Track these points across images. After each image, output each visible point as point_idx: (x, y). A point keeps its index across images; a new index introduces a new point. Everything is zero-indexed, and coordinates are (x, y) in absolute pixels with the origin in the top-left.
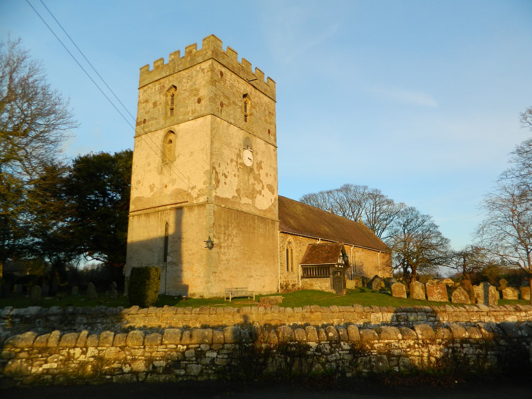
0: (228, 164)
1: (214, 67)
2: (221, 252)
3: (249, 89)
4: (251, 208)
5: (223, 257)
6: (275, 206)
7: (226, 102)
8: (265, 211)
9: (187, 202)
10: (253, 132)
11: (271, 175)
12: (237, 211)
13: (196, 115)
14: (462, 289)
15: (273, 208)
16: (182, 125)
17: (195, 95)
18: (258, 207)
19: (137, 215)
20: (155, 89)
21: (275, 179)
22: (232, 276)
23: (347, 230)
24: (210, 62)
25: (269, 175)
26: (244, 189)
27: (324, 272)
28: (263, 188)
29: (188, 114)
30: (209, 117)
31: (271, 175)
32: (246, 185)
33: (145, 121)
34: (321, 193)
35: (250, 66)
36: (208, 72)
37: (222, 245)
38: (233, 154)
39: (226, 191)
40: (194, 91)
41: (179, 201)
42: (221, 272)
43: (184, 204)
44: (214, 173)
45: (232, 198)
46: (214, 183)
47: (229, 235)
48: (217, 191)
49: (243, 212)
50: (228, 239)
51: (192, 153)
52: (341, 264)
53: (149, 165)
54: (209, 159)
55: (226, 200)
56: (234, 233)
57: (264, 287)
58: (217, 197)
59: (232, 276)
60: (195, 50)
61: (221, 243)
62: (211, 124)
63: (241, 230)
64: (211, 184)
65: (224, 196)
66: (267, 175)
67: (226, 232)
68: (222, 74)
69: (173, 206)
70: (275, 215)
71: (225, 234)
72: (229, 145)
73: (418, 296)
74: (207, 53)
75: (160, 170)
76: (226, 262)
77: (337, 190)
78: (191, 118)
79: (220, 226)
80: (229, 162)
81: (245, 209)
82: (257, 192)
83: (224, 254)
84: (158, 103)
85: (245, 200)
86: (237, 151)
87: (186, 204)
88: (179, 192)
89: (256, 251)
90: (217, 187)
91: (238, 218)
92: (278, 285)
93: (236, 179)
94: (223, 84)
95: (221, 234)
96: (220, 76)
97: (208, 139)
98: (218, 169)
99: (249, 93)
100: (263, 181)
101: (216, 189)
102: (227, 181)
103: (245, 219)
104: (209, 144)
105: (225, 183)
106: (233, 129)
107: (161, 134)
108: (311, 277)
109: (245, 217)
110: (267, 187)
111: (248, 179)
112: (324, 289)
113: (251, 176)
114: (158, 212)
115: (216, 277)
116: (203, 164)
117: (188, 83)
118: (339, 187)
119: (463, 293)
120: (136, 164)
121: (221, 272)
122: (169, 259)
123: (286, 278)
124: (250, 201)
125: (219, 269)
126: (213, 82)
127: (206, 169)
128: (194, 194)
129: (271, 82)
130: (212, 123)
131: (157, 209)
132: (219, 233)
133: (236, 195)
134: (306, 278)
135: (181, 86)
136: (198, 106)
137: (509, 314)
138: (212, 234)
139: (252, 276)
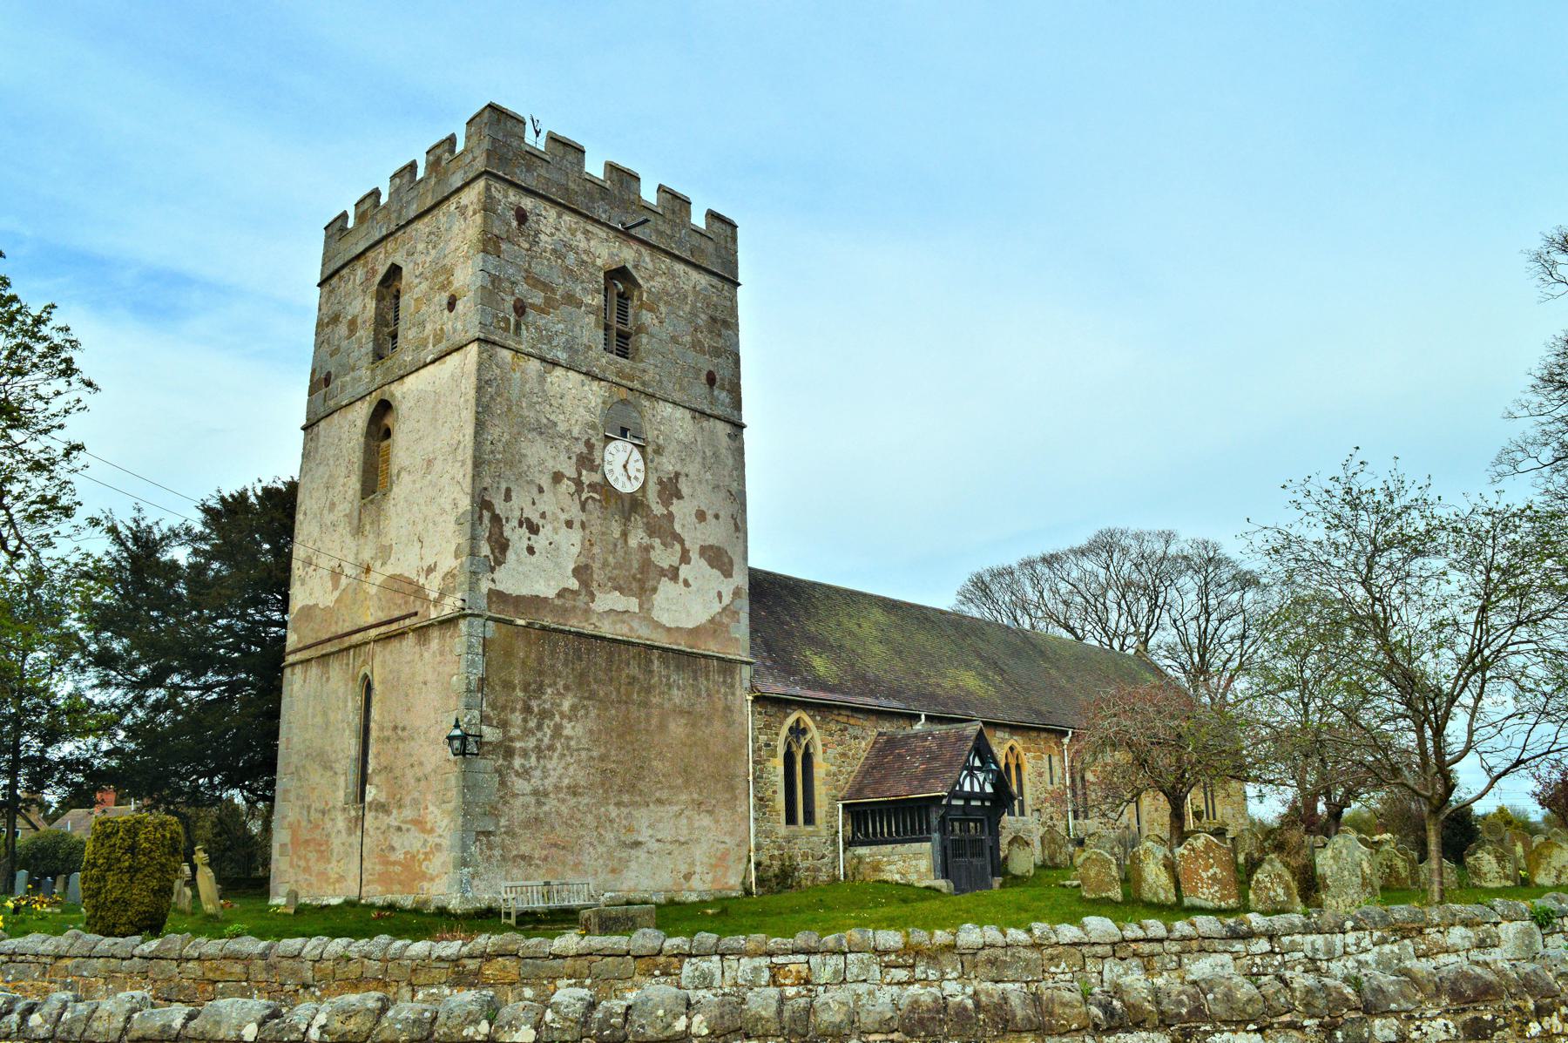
0: (541, 490)
2: (510, 767)
3: (627, 254)
4: (635, 624)
5: (519, 785)
6: (736, 613)
7: (537, 298)
8: (695, 632)
10: (643, 384)
11: (717, 517)
12: (579, 635)
13: (443, 346)
14: (1278, 865)
15: (725, 620)
17: (443, 287)
18: (666, 619)
19: (302, 662)
22: (555, 845)
23: (1063, 682)
24: (481, 183)
25: (709, 517)
26: (605, 564)
27: (913, 825)
29: (426, 346)
31: (717, 517)
32: (614, 552)
33: (327, 381)
34: (1030, 564)
37: (518, 745)
38: (563, 456)
39: (538, 573)
41: (397, 614)
42: (510, 832)
43: (407, 622)
44: (486, 521)
45: (559, 595)
46: (485, 550)
47: (545, 715)
48: (496, 575)
49: (603, 638)
50: (539, 727)
51: (430, 462)
52: (982, 796)
54: (469, 479)
55: (536, 603)
56: (566, 705)
57: (688, 877)
58: (497, 596)
59: (555, 845)
61: (512, 740)
63: (592, 696)
65: (525, 591)
66: (701, 516)
67: (534, 704)
68: (522, 216)
69: (383, 629)
70: (738, 641)
71: (527, 709)
72: (545, 430)
73: (1156, 894)
75: (356, 522)
76: (533, 800)
77: (1074, 552)
79: (508, 686)
80: (545, 482)
81: (607, 629)
82: (662, 573)
83: (525, 773)
84: (359, 321)
85: (608, 600)
89: (655, 763)
90: (499, 563)
91: (580, 659)
92: (747, 870)
93: (576, 536)
94: (527, 246)
95: (513, 710)
96: (515, 224)
97: (468, 416)
98: (500, 507)
99: (629, 266)
100: (685, 536)
101: (492, 570)
102: (540, 542)
103: (610, 661)
104: (469, 430)
105: (531, 550)
108: (886, 842)
109: (611, 654)
111: (625, 535)
112: (912, 878)
113: (638, 520)
114: (348, 649)
115: (490, 847)
116: (453, 492)
118: (1081, 541)
119: (1280, 876)
121: (510, 832)
122: (371, 793)
123: (780, 848)
124: (633, 604)
125: (503, 822)
126: (490, 244)
127: (461, 511)
128: (432, 586)
129: (717, 225)
130: (480, 365)
131: (347, 642)
132: (504, 708)
133: (574, 584)
134: (863, 844)
136: (449, 322)
137: (1202, 950)
138: (476, 713)
139: (637, 844)
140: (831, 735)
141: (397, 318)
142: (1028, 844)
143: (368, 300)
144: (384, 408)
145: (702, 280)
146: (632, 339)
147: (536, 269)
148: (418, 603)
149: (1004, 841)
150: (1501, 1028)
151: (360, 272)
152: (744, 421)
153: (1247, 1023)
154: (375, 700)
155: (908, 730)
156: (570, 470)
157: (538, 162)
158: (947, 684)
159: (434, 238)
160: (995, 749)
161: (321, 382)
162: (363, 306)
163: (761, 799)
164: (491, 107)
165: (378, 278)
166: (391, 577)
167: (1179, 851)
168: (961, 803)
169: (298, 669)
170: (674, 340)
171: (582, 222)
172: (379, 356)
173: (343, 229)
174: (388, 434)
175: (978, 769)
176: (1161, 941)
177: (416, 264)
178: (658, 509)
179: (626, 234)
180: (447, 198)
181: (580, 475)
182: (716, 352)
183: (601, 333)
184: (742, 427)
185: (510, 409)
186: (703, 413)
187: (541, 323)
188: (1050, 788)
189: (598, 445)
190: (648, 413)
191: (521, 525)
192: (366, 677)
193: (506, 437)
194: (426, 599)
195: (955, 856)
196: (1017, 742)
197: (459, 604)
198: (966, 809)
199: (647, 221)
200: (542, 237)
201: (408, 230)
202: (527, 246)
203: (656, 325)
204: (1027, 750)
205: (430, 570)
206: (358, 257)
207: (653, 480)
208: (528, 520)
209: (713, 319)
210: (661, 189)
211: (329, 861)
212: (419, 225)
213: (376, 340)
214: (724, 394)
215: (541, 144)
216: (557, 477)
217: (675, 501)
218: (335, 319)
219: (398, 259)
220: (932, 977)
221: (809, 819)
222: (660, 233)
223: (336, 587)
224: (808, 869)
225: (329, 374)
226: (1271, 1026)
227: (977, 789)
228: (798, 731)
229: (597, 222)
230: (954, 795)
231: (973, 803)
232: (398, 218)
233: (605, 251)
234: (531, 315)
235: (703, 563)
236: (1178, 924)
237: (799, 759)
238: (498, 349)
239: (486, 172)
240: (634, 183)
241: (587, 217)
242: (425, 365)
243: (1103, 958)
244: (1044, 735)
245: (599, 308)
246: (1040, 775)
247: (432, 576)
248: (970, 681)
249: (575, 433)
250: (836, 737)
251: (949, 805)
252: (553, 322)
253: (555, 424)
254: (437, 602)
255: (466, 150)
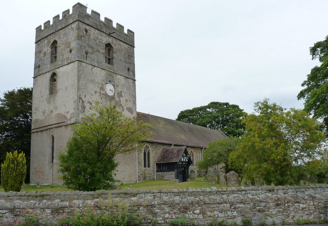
0: (92, 95)
1: (79, 26)
3: (110, 40)
7: (90, 50)
9: (64, 122)
10: (114, 71)
11: (130, 101)
13: (69, 61)
16: (61, 69)
17: (68, 47)
19: (36, 132)
20: (45, 43)
21: (134, 104)
24: (77, 23)
25: (128, 101)
28: (123, 110)
29: (64, 61)
30: (77, 62)
31: (130, 101)
33: (39, 67)
35: (111, 22)
36: (76, 30)
40: (68, 44)
41: (60, 122)
43: (62, 124)
52: (185, 162)
53: (42, 97)
54: (76, 93)
57: (124, 178)
60: (68, 14)
62: (78, 68)
64: (78, 109)
66: (126, 101)
68: (86, 31)
69: (56, 125)
72: (93, 81)
74: (75, 16)
78: (66, 64)
80: (93, 93)
84: (47, 53)
86: (101, 85)
87: (64, 123)
88: (59, 115)
94: (88, 38)
96: (85, 32)
97: (76, 78)
99: (111, 43)
104: (76, 81)
106: (96, 70)
107: (49, 75)
110: (127, 109)
114: (48, 129)
116: (73, 95)
117: (64, 38)
120: (34, 96)
126: (79, 37)
127: (75, 100)
128: (68, 116)
129: (130, 33)
130: (78, 67)
134: (160, 172)
135: (60, 41)
140: (154, 149)
141: (56, 53)
142: (194, 172)
143: (49, 48)
144: (54, 74)
145: (126, 46)
146: (111, 60)
147: (90, 43)
148: (65, 120)
149: (190, 171)
150: (281, 205)
151: (46, 41)
152: (136, 79)
153: (242, 203)
154: (55, 140)
155: (170, 148)
156: (98, 91)
157: (90, 17)
158: (178, 137)
159: (66, 35)
160: (188, 151)
161: (37, 67)
162: (48, 50)
163: (139, 162)
164: (79, 4)
165: (51, 43)
166: (57, 114)
167: (227, 174)
168: (185, 163)
169: (35, 133)
170: (121, 60)
171: (100, 32)
172: (52, 62)
173: (41, 30)
174: (55, 80)
175: (185, 156)
176: (225, 191)
177: (61, 40)
178: (117, 99)
179: (109, 35)
180: (68, 25)
181: (100, 92)
182: (130, 63)
183: (105, 59)
184: (135, 80)
185: (85, 77)
186: (127, 77)
187: (91, 56)
188: (199, 160)
189: (104, 85)
190: (115, 77)
191: (88, 103)
192: (52, 135)
193: (85, 83)
194: (67, 119)
195: (180, 174)
196: (192, 150)
197: (75, 120)
198: (182, 165)
199: (114, 32)
200: (91, 36)
201: (58, 32)
202: (88, 38)
203: (117, 57)
204: (194, 152)
205: (68, 112)
206: (45, 37)
207: (116, 93)
208: (89, 102)
209: (129, 55)
210: (117, 24)
211: (45, 176)
212: (61, 31)
213: (51, 58)
214: (131, 73)
215: (90, 13)
216: (96, 92)
217: (121, 97)
218: (40, 52)
219: (56, 39)
220: (183, 197)
221: (149, 166)
222: (117, 35)
223: (44, 115)
224: (148, 177)
225: (39, 65)
226: (245, 203)
227: (184, 160)
228: (147, 147)
229: (103, 32)
230: (180, 162)
231: (183, 163)
232: (56, 28)
233: (106, 39)
234: (89, 55)
235: (127, 111)
236: (229, 188)
237: (147, 154)
238: (82, 63)
239: (78, 20)
240: (111, 22)
241: (101, 31)
242: (65, 65)
243: (215, 194)
244: (198, 149)
245: (104, 53)
246: (197, 157)
247: (68, 114)
248: (183, 137)
249: (99, 82)
250: (154, 149)
251: (179, 164)
252: (93, 56)
253: (95, 80)
254: (69, 120)
255: (73, 13)
